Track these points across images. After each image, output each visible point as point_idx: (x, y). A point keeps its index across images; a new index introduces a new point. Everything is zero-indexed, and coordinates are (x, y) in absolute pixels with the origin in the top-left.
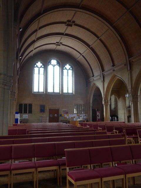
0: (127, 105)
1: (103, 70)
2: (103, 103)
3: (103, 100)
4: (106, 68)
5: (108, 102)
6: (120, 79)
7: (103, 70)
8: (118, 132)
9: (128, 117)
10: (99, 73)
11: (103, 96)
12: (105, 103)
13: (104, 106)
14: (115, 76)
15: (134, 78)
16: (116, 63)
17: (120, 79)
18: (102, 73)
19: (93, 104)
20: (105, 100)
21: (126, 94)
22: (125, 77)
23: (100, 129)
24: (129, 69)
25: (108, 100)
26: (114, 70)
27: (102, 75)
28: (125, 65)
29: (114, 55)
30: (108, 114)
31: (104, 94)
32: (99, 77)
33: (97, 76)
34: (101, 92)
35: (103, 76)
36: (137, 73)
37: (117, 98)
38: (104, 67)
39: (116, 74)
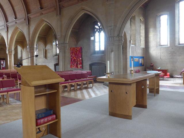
0: (54, 53)
1: (7, 21)
2: (7, 52)
3: (7, 49)
4: (11, 18)
5: (11, 52)
6: (50, 25)
7: (7, 21)
8: (7, 77)
9: (90, 66)
10: (4, 24)
11: (7, 46)
12: (9, 52)
13: (8, 55)
14: (17, 29)
15: (31, 32)
16: (18, 16)
17: (50, 25)
18: (58, 4)
19: (15, 52)
20: (9, 50)
21: (54, 42)
22: (54, 22)
23: (5, 77)
24: (27, 24)
25: (11, 50)
26: (16, 23)
27: (6, 25)
28: (25, 19)
29: (16, 8)
30: (12, 63)
31: (8, 45)
32: (3, 27)
33: (12, 22)
34: (26, 38)
35: (7, 26)
36: (33, 29)
37: (22, 49)
38: (8, 18)
39: (43, 19)
